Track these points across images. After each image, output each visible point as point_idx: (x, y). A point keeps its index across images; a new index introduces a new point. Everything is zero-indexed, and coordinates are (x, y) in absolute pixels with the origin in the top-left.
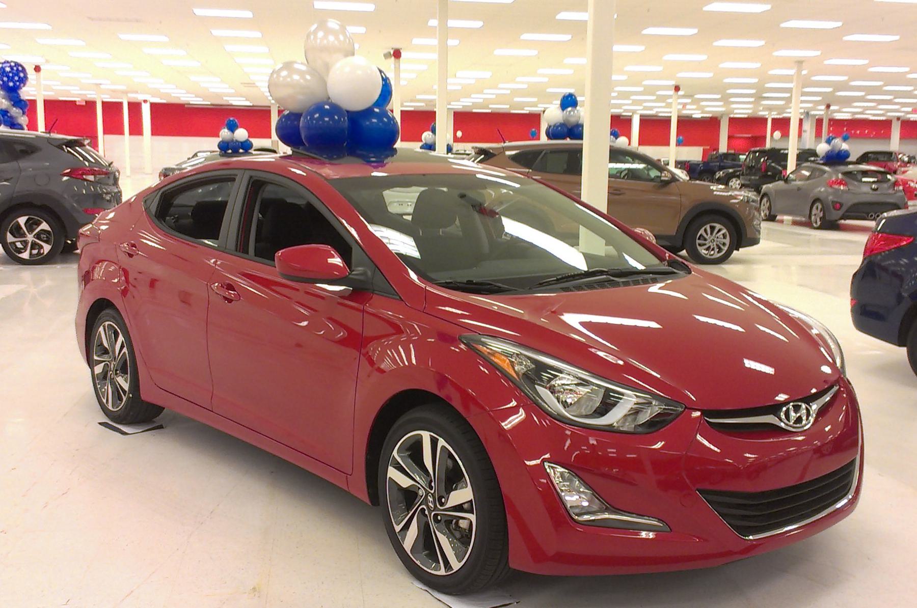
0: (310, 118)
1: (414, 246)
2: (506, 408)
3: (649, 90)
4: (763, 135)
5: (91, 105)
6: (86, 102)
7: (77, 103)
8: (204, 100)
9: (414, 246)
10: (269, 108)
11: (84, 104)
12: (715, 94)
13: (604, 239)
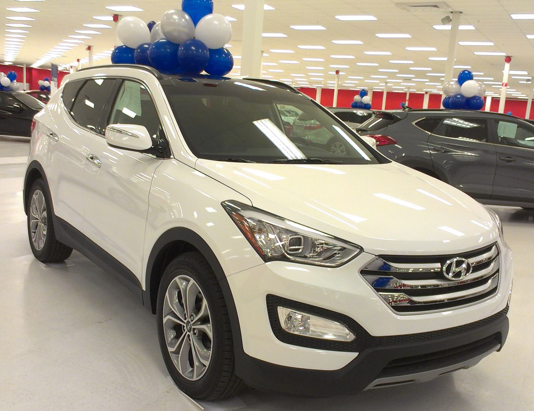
5: (405, 94)
10: (499, 99)
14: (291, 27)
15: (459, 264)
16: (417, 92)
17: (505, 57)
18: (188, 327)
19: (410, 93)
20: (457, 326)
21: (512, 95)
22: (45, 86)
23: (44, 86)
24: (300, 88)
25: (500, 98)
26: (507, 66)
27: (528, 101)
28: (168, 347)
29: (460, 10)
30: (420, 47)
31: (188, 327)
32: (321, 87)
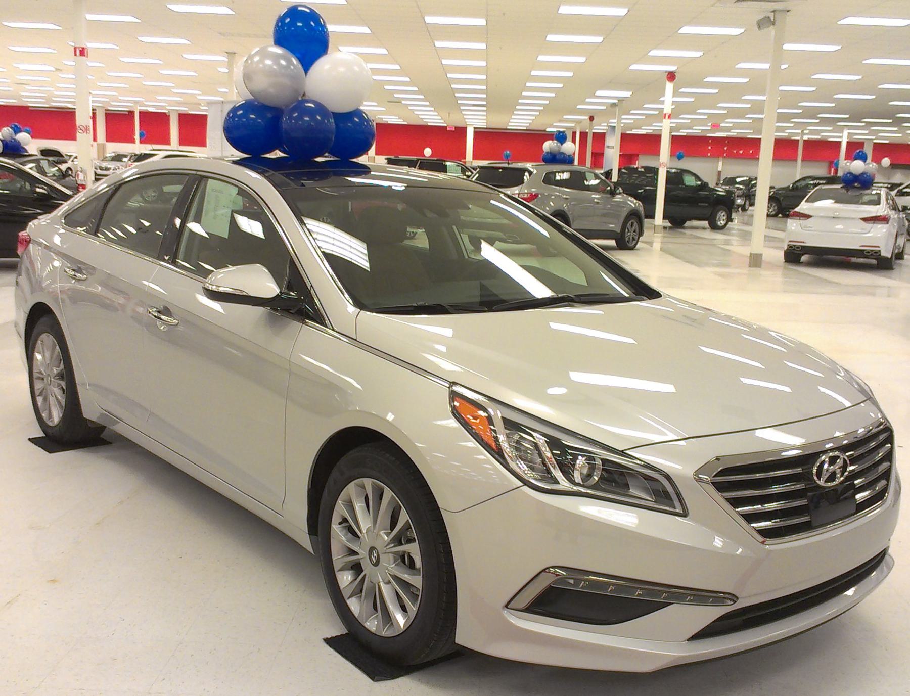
0: (232, 116)
1: (365, 254)
2: (192, 266)
3: (811, 113)
4: (602, 152)
5: (131, 113)
6: (455, 128)
7: (448, 129)
8: (404, 121)
9: (365, 254)
10: (73, 110)
11: (454, 130)
12: (845, 114)
13: (671, 384)
14: (864, 62)
15: (833, 461)
16: (190, 112)
17: (667, 74)
18: (375, 555)
19: (140, 112)
20: (815, 585)
21: (384, 120)
22: (854, 173)
23: (851, 174)
24: (127, 113)
25: (75, 109)
26: (669, 86)
27: (77, 112)
28: (421, 589)
29: (788, 9)
30: (369, 46)
31: (375, 555)
32: (177, 110)
